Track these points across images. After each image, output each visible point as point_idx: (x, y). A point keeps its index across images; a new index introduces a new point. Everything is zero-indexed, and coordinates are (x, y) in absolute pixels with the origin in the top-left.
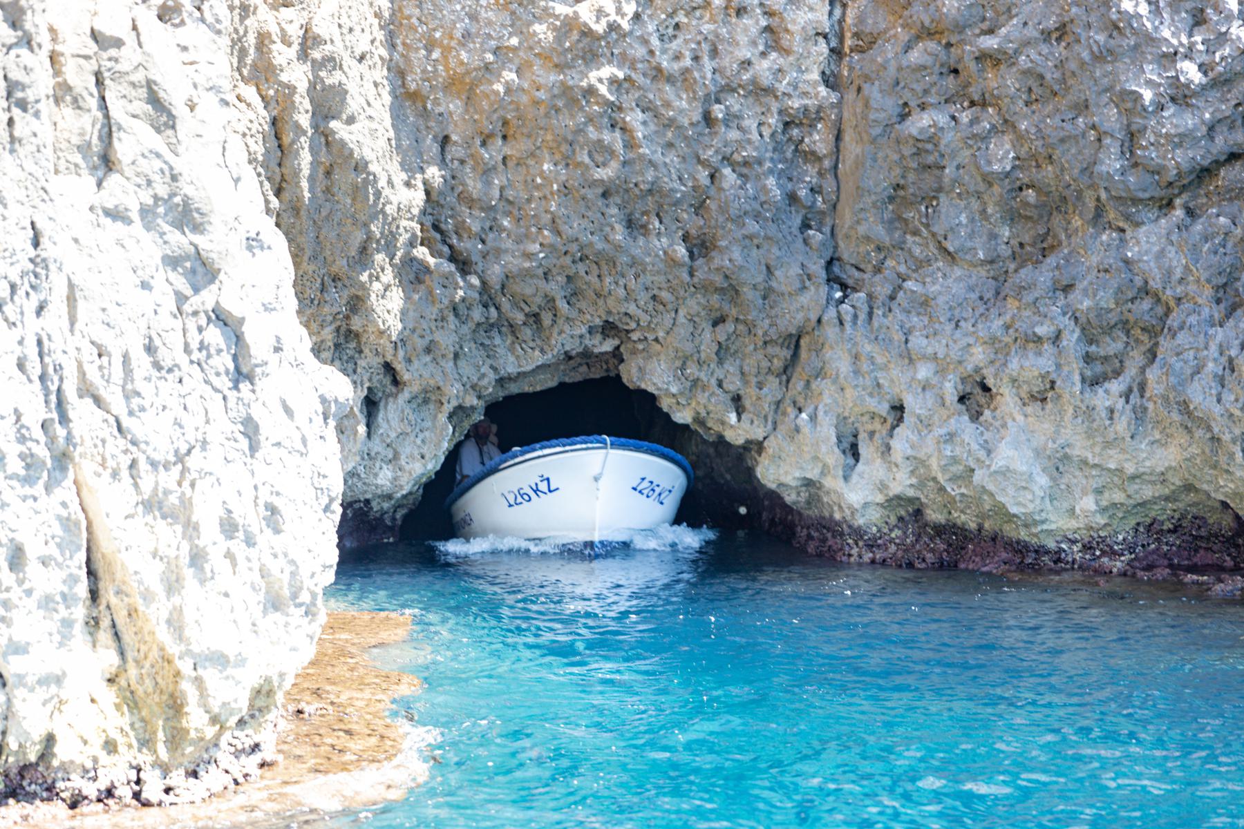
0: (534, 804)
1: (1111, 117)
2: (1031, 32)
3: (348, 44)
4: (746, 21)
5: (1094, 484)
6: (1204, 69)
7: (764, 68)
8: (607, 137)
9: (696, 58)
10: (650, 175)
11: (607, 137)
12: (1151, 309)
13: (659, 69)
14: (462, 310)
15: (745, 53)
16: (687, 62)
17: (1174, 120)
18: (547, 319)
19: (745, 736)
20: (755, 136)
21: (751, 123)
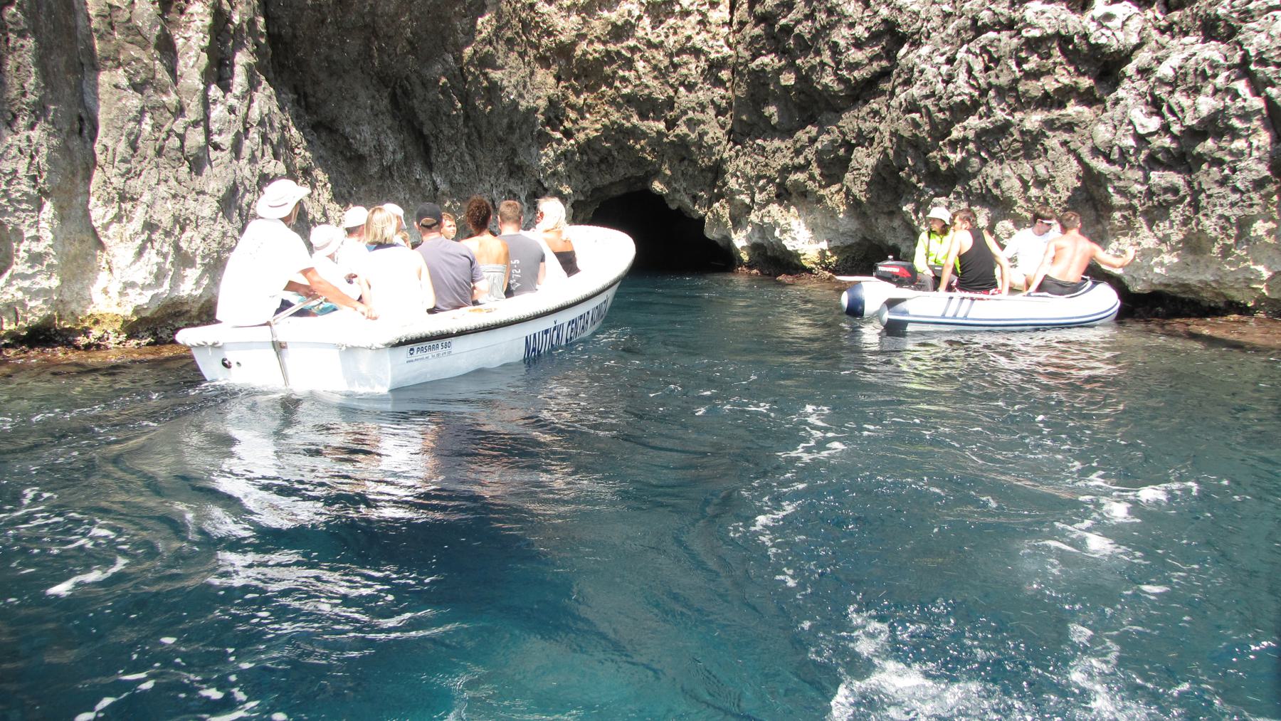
0: (523, 422)
1: (827, 56)
2: (800, 16)
3: (113, 211)
4: (691, 18)
5: (829, 236)
6: (868, 29)
7: (697, 41)
8: (627, 74)
9: (667, 36)
10: (646, 91)
11: (627, 74)
12: (858, 145)
13: (649, 41)
14: (569, 155)
15: (688, 33)
16: (663, 38)
17: (856, 55)
18: (610, 159)
19: (958, 418)
20: (694, 72)
21: (692, 66)
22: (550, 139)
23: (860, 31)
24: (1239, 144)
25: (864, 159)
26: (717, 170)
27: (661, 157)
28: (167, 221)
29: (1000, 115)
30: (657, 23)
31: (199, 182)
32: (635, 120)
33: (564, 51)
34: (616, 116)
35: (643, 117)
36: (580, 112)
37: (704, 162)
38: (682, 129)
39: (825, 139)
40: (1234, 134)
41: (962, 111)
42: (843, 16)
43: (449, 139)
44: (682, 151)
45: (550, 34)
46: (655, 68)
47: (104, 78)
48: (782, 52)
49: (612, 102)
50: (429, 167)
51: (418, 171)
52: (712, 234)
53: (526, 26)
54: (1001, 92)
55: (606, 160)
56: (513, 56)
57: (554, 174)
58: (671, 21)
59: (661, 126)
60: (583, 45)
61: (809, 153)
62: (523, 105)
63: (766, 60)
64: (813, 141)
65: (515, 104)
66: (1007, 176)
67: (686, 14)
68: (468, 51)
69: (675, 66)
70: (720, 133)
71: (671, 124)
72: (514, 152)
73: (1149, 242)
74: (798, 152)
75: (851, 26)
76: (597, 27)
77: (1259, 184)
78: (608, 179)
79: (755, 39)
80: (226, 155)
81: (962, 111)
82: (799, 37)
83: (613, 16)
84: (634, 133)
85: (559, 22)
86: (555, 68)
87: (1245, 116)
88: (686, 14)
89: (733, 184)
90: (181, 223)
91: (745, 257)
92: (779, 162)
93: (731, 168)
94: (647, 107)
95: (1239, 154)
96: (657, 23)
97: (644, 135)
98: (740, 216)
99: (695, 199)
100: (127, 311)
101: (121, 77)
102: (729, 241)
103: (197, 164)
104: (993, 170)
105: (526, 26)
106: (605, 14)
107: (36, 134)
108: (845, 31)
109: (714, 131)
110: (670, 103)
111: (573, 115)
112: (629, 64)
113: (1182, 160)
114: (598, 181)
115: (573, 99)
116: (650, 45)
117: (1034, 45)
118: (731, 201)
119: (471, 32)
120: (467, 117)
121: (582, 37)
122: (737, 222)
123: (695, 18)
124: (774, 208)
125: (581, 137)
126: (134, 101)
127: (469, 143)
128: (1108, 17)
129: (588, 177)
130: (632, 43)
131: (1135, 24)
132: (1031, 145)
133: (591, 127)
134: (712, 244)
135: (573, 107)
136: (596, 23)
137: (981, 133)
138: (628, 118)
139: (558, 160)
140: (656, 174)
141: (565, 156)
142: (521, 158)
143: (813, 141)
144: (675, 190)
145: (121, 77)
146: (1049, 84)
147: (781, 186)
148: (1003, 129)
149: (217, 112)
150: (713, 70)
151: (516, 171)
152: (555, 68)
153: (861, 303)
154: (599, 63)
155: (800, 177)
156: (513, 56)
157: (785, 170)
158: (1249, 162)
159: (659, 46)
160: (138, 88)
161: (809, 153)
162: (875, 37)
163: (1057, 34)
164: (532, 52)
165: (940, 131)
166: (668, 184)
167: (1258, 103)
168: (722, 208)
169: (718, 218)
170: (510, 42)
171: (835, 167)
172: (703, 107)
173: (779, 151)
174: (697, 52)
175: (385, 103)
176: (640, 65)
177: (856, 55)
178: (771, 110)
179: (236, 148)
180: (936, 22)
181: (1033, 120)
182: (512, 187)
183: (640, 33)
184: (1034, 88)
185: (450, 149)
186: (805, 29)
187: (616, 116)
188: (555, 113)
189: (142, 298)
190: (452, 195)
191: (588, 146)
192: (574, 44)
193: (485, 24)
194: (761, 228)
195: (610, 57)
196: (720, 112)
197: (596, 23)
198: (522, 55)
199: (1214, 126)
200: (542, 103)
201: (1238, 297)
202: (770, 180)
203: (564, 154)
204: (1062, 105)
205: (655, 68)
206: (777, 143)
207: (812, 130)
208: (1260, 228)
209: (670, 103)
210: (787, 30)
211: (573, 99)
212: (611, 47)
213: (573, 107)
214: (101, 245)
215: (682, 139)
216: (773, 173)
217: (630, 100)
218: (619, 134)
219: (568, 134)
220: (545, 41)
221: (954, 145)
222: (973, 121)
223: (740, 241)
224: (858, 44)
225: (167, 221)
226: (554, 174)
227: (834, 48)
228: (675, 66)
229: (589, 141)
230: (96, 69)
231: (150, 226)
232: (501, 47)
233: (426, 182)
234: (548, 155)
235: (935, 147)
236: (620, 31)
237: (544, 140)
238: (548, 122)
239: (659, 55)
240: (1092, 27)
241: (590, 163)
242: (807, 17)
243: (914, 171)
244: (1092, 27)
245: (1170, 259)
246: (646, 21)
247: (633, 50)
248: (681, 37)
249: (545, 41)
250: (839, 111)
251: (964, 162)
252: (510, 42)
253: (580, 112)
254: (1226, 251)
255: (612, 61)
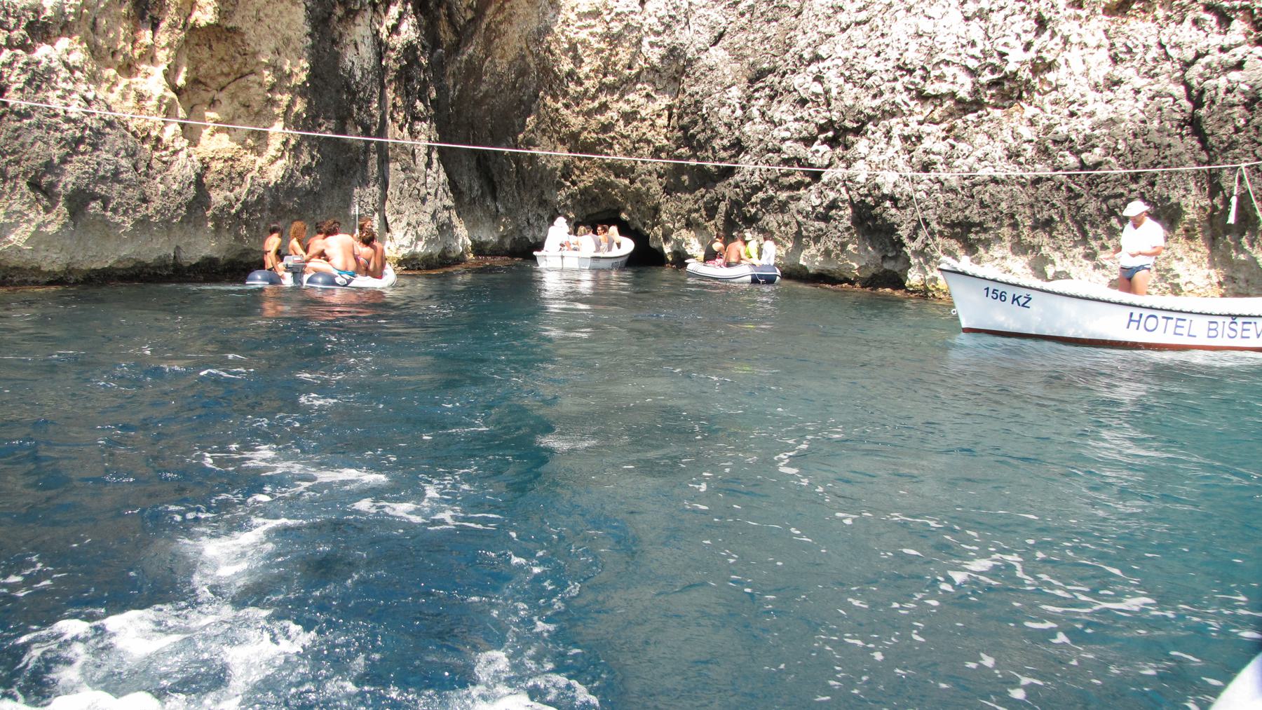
1: (710, 153)
7: (649, 135)
17: (723, 154)
22: (563, 186)
23: (725, 142)
24: (841, 213)
25: (723, 207)
26: (656, 210)
27: (626, 199)
28: (414, 223)
29: (771, 193)
30: (627, 124)
31: (424, 208)
32: (612, 177)
33: (574, 136)
34: (601, 175)
35: (617, 176)
36: (582, 171)
37: (650, 204)
38: (638, 185)
39: (708, 196)
40: (841, 209)
41: (756, 189)
42: (718, 133)
43: (508, 184)
44: (638, 198)
45: (566, 126)
46: (625, 149)
47: (391, 165)
48: (691, 148)
49: (600, 167)
50: (495, 199)
51: (489, 202)
52: (654, 245)
53: (553, 121)
54: (772, 182)
55: (595, 199)
56: (545, 138)
57: (565, 205)
58: (635, 123)
59: (627, 182)
60: (585, 134)
61: (701, 203)
62: (549, 166)
63: (683, 150)
64: (703, 196)
65: (544, 165)
66: (771, 220)
67: (643, 120)
68: (521, 136)
69: (636, 149)
70: (659, 188)
71: (632, 182)
72: (543, 193)
73: (814, 252)
74: (696, 202)
75: (722, 139)
76: (593, 124)
77: (848, 229)
78: (596, 210)
79: (678, 138)
80: (432, 198)
81: (756, 189)
82: (699, 141)
83: (602, 119)
84: (611, 185)
85: (572, 120)
86: (568, 145)
87: (843, 202)
88: (643, 120)
89: (664, 217)
90: (419, 224)
91: (670, 258)
92: (688, 206)
93: (663, 208)
94: (619, 170)
95: (841, 217)
96: (627, 124)
97: (617, 186)
98: (667, 238)
99: (644, 224)
100: (400, 256)
101: (398, 166)
102: (661, 248)
103: (424, 201)
104: (767, 218)
105: (553, 121)
106: (598, 117)
107: (375, 188)
108: (718, 141)
109: (656, 187)
110: (632, 169)
111: (577, 173)
112: (611, 146)
113: (825, 218)
114: (590, 211)
115: (577, 163)
116: (623, 136)
117: (786, 162)
118: (663, 226)
119: (523, 125)
120: (518, 172)
121: (584, 129)
122: (667, 238)
123: (648, 123)
124: (684, 231)
125: (581, 185)
126: (402, 176)
127: (518, 186)
128: (817, 151)
129: (584, 208)
130: (612, 134)
131: (827, 156)
132: (783, 208)
133: (587, 180)
134: (654, 250)
135: (578, 168)
136: (592, 122)
137: (763, 200)
138: (608, 176)
139: (567, 198)
140: (624, 209)
141: (572, 196)
142: (546, 196)
143: (703, 196)
144: (633, 219)
145: (398, 166)
146: (792, 180)
147: (688, 219)
148: (771, 199)
149: (429, 180)
150: (657, 153)
151: (543, 203)
152: (568, 145)
153: (34, 51)
154: (594, 144)
155: (695, 215)
156: (545, 138)
157: (690, 211)
158: (844, 220)
159: (627, 137)
160: (403, 170)
161: (701, 203)
162: (732, 146)
163: (795, 158)
164: (555, 136)
165: (748, 198)
166: (629, 215)
167: (847, 197)
168: (658, 231)
169: (656, 235)
170: (544, 131)
171: (711, 212)
172: (650, 174)
173: (687, 201)
174: (648, 142)
175: (474, 163)
176: (616, 147)
177: (723, 154)
178: (685, 178)
179: (436, 194)
180: (756, 143)
181: (783, 196)
182: (540, 212)
183: (617, 129)
184: (786, 181)
185: (507, 189)
186: (701, 137)
187: (601, 175)
188: (567, 171)
189: (405, 251)
190: (506, 215)
191: (584, 192)
192: (580, 133)
193: (531, 121)
194: (679, 243)
195: (600, 142)
196: (660, 176)
197: (592, 122)
198: (550, 138)
199: (833, 205)
200: (560, 165)
201: (848, 276)
202: (683, 216)
203: (571, 195)
204: (798, 189)
205: (625, 149)
206: (687, 196)
207: (703, 190)
208: (850, 247)
209: (632, 169)
210: (693, 136)
211: (577, 163)
212: (601, 136)
213: (578, 168)
214: (388, 230)
215: (638, 190)
216: (683, 212)
217: (610, 166)
218: (603, 185)
219: (574, 183)
220: (563, 129)
221: (753, 205)
222: (761, 195)
223: (667, 249)
224: (725, 149)
225: (414, 223)
226: (565, 205)
227: (713, 148)
228: (636, 149)
229: (586, 188)
230: (388, 162)
231: (409, 224)
232: (539, 134)
233: (492, 207)
234: (561, 195)
235: (745, 205)
236: (606, 128)
237: (560, 186)
238: (563, 176)
239: (628, 142)
240: (810, 155)
241: (586, 200)
242: (703, 131)
243: (737, 216)
244: (810, 155)
245: (819, 259)
246: (621, 123)
247: (613, 138)
248: (640, 133)
249: (563, 129)
250: (715, 182)
251: (756, 213)
252: (544, 131)
253: (582, 171)
254: (837, 256)
255: (601, 144)
